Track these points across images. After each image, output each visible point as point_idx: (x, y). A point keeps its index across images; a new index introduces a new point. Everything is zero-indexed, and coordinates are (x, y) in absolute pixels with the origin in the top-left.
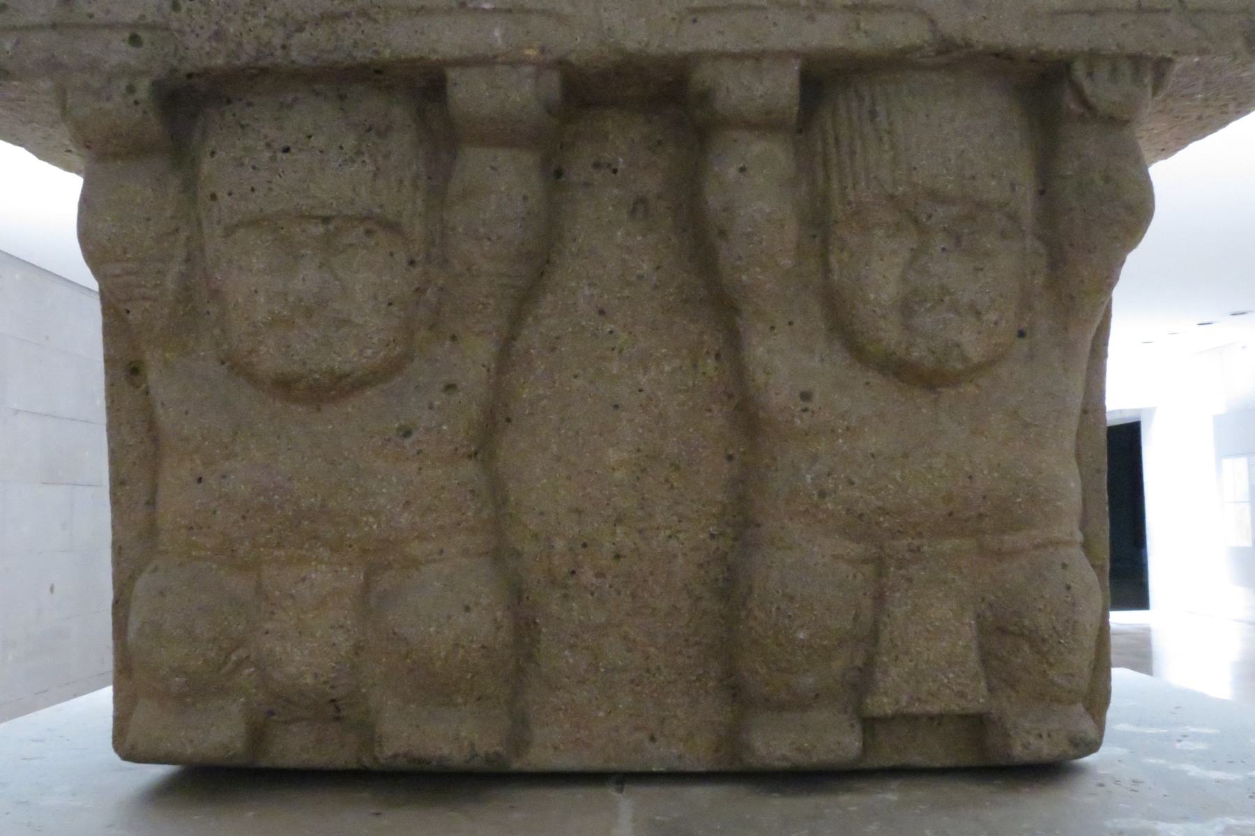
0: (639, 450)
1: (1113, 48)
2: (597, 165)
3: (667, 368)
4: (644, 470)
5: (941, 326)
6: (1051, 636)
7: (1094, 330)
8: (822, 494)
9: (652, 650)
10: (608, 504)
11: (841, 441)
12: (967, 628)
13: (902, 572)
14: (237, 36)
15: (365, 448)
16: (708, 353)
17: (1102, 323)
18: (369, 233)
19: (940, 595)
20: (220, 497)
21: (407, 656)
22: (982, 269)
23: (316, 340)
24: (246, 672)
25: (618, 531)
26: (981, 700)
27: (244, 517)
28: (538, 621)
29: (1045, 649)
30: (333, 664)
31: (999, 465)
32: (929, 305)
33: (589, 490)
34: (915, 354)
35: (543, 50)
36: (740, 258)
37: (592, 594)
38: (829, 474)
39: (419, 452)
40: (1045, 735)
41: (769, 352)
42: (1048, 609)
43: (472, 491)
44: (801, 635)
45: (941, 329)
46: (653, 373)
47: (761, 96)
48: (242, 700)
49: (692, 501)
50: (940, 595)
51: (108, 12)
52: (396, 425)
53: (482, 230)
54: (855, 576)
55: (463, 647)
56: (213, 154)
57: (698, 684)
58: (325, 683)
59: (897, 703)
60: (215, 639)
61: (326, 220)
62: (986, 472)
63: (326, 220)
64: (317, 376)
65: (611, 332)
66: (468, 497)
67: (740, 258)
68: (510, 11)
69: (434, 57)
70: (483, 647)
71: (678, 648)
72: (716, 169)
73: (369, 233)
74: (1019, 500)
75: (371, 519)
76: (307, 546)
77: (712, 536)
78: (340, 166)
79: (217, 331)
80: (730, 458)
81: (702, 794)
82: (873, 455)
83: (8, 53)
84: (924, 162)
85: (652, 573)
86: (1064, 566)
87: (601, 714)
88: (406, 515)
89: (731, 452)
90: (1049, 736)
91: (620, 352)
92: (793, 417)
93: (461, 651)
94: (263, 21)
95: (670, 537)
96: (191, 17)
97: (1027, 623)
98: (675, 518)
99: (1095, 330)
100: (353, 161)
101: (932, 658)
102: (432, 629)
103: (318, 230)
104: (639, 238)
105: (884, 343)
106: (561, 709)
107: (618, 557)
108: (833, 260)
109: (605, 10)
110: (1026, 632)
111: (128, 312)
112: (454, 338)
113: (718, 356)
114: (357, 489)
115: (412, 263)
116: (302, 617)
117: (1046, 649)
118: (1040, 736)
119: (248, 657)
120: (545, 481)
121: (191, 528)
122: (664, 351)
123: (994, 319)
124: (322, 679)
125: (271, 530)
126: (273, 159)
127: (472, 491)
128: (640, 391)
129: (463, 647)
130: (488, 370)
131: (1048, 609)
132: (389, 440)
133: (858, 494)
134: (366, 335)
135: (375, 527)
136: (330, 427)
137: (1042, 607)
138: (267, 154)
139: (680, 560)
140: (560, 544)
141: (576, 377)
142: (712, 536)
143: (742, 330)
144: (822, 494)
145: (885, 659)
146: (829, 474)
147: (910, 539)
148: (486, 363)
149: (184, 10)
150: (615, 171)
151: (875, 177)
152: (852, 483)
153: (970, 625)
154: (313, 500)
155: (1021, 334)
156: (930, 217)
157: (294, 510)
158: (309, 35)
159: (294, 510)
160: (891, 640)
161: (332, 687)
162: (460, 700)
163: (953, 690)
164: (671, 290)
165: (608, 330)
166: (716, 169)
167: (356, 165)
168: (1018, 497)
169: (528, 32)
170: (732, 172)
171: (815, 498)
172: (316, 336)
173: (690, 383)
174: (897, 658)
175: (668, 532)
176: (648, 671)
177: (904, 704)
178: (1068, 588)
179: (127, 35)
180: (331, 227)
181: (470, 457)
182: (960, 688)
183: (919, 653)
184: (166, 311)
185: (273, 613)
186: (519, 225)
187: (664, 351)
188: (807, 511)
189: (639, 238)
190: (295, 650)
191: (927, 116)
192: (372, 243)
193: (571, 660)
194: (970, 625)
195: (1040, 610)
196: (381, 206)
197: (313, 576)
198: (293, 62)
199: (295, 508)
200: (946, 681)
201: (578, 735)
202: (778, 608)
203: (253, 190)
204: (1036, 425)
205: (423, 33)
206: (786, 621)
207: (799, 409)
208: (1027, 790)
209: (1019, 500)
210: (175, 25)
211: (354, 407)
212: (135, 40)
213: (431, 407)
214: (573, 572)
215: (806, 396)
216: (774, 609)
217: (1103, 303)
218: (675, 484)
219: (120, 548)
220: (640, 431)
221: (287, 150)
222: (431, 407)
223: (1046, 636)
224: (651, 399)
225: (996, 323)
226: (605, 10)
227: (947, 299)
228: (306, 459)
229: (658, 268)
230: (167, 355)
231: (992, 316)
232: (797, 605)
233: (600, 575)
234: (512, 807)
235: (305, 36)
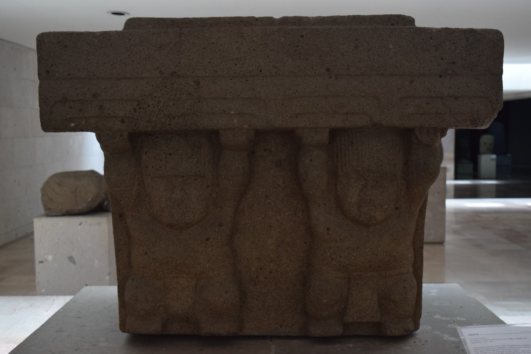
0: (277, 240)
1: (427, 126)
2: (265, 150)
3: (287, 214)
4: (279, 246)
5: (369, 211)
6: (399, 301)
7: (422, 202)
8: (332, 259)
9: (281, 300)
10: (268, 257)
11: (338, 243)
12: (375, 298)
13: (356, 282)
14: (155, 122)
15: (195, 244)
16: (299, 210)
17: (423, 205)
18: (195, 179)
19: (367, 288)
20: (153, 259)
21: (209, 306)
22: (384, 192)
23: (181, 213)
24: (161, 309)
25: (271, 265)
26: (378, 318)
27: (160, 265)
28: (246, 292)
29: (397, 305)
30: (188, 307)
31: (386, 251)
32: (366, 204)
33: (262, 252)
34: (361, 219)
35: (249, 126)
36: (309, 187)
37: (263, 284)
38: (334, 253)
39: (212, 245)
40: (397, 329)
41: (318, 213)
42: (398, 294)
43: (227, 256)
44: (324, 301)
45: (369, 212)
46: (282, 216)
47: (317, 140)
48: (160, 317)
49: (294, 256)
50: (367, 288)
51: (114, 113)
52: (205, 237)
53: (230, 178)
54: (342, 283)
55: (226, 303)
56: (146, 153)
57: (295, 311)
58: (185, 312)
59: (353, 319)
60: (153, 301)
61: (183, 177)
62: (382, 253)
63: (183, 177)
64: (182, 225)
65: (269, 202)
66: (226, 258)
67: (309, 187)
68: (239, 114)
69: (216, 128)
70: (232, 303)
71: (289, 300)
72: (303, 159)
73: (195, 179)
74: (391, 262)
75: (198, 266)
76: (179, 273)
77: (300, 267)
78: (187, 160)
79: (148, 206)
80: (306, 243)
81: (295, 343)
82: (348, 248)
83: (83, 125)
84: (367, 160)
85: (281, 277)
86: (404, 281)
87: (266, 319)
88: (208, 264)
89: (306, 241)
90: (398, 329)
91: (272, 209)
92: (324, 235)
93: (226, 305)
94: (162, 116)
95: (287, 266)
96: (140, 114)
97: (392, 297)
98: (288, 261)
99: (420, 207)
100: (191, 158)
101: (364, 306)
102: (217, 298)
103: (180, 180)
104: (278, 173)
105: (352, 214)
106: (254, 318)
107: (271, 272)
108: (338, 187)
109: (269, 114)
110: (392, 300)
111: (121, 201)
112: (221, 207)
113: (302, 211)
114: (194, 257)
115: (208, 186)
116: (178, 294)
117: (397, 305)
118: (395, 329)
119: (162, 305)
120: (249, 249)
121: (144, 268)
122: (286, 209)
123: (386, 207)
124: (184, 312)
125: (168, 269)
126: (166, 157)
127: (227, 256)
128: (278, 221)
129: (226, 303)
130: (231, 218)
131: (398, 294)
132: (203, 242)
133: (343, 260)
134: (196, 211)
135: (199, 268)
136: (184, 237)
137: (396, 293)
138: (164, 156)
139: (290, 274)
140: (253, 268)
141: (258, 217)
142: (300, 267)
143: (310, 206)
144: (332, 259)
145: (350, 306)
146: (334, 253)
147: (358, 273)
148: (231, 216)
149: (138, 112)
150: (271, 152)
151: (351, 164)
152: (341, 256)
153: (376, 297)
154: (181, 260)
155: (397, 208)
156: (368, 177)
157: (175, 264)
158: (177, 120)
159: (175, 264)
160: (352, 301)
161: (187, 314)
162: (224, 317)
163: (370, 316)
164: (288, 190)
165: (268, 202)
166: (303, 159)
167: (192, 159)
168: (391, 261)
169: (245, 120)
170: (308, 161)
171: (330, 260)
172: (181, 212)
173: (294, 219)
174: (353, 306)
175: (286, 265)
176: (280, 306)
177: (355, 319)
178: (405, 287)
179: (120, 119)
180: (185, 179)
181: (226, 245)
182: (372, 315)
183: (360, 305)
184: (133, 201)
185: (169, 293)
186: (242, 176)
187: (286, 209)
188: (327, 264)
189: (278, 173)
190: (176, 303)
191: (368, 145)
192: (197, 182)
193: (257, 303)
194: (376, 297)
195: (396, 294)
196: (199, 172)
197: (181, 282)
198: (172, 129)
199: (176, 263)
200: (368, 313)
201: (259, 325)
202: (318, 293)
203: (160, 167)
204: (398, 239)
205: (212, 121)
206: (320, 297)
207: (326, 233)
208: (392, 344)
209: (391, 262)
210: (136, 117)
211: (191, 231)
212: (123, 121)
213: (215, 232)
214: (257, 277)
215: (328, 229)
216: (317, 293)
217: (423, 200)
218: (289, 250)
219: (119, 270)
220: (278, 234)
221: (170, 154)
222: (215, 232)
223: (398, 301)
224: (282, 224)
225: (387, 209)
226: (269, 114)
227: (372, 202)
228: (178, 248)
229: (284, 183)
230: (133, 214)
231: (386, 207)
232: (324, 293)
233: (266, 278)
234: (240, 347)
235: (176, 120)
